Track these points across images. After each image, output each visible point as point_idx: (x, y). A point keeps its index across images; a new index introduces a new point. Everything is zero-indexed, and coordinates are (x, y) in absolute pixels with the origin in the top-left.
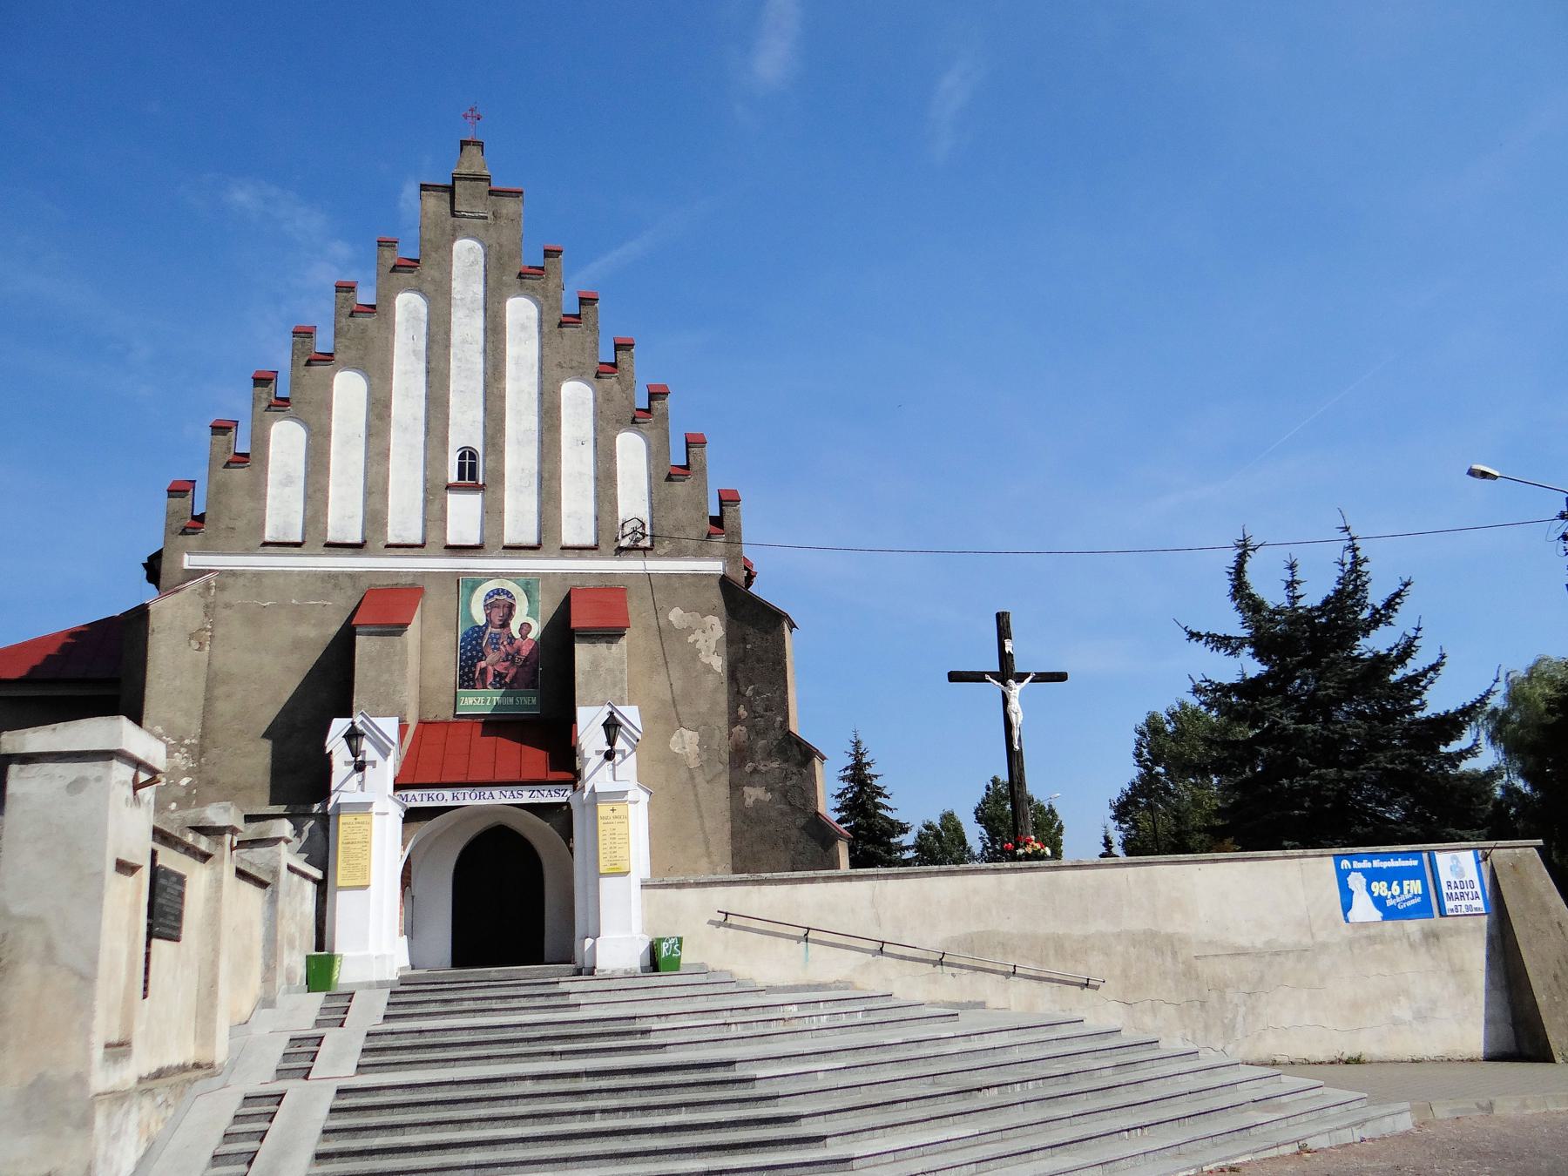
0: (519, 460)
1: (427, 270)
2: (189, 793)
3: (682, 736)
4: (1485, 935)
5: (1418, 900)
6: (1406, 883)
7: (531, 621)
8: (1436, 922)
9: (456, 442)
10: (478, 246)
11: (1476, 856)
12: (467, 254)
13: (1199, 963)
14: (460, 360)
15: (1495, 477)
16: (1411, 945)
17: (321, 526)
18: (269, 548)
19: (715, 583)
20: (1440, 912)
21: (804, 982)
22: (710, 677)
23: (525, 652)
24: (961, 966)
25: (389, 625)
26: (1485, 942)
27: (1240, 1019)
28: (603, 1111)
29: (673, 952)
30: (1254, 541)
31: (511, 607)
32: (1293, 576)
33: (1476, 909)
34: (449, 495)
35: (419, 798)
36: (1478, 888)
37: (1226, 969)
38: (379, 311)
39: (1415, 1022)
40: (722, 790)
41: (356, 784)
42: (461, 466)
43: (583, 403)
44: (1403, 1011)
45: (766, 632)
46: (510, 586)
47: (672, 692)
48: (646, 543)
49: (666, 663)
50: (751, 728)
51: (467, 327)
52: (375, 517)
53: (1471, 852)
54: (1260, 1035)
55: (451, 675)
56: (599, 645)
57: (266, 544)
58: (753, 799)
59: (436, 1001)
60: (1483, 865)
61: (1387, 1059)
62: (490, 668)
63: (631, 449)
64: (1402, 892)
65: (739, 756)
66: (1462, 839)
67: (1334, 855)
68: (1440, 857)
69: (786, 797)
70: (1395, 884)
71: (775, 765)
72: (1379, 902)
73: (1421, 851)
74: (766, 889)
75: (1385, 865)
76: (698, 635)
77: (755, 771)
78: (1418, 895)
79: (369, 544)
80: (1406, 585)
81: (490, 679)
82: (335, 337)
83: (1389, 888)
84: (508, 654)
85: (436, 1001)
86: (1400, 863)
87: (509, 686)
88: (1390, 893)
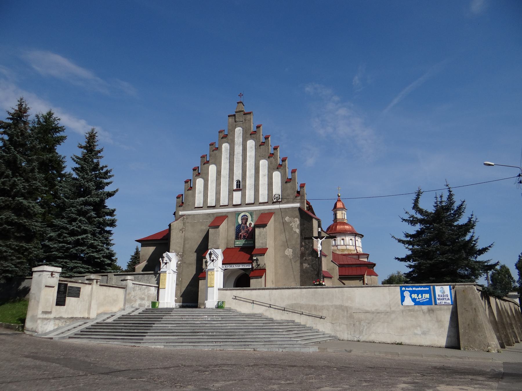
0: (250, 182)
1: (229, 137)
2: (180, 265)
3: (288, 250)
4: (451, 311)
5: (428, 300)
6: (424, 295)
7: (252, 222)
8: (433, 306)
9: (236, 178)
10: (241, 128)
11: (450, 287)
12: (238, 130)
13: (354, 314)
14: (237, 158)
15: (493, 165)
16: (423, 313)
17: (206, 202)
18: (196, 209)
19: (297, 209)
20: (435, 303)
21: (252, 313)
22: (296, 235)
23: (250, 230)
24: (289, 311)
25: (215, 226)
26: (450, 313)
27: (365, 330)
28: (124, 329)
29: (221, 304)
30: (422, 191)
31: (247, 219)
32: (441, 200)
33: (448, 303)
34: (234, 192)
35: (227, 267)
36: (449, 297)
37: (362, 316)
38: (218, 149)
39: (421, 335)
40: (298, 264)
41: (165, 267)
42: (237, 185)
43: (265, 165)
44: (418, 331)
45: (309, 222)
46: (247, 214)
47: (286, 239)
48: (280, 200)
49: (285, 231)
50: (305, 248)
51: (238, 149)
52: (218, 199)
53: (448, 286)
54: (370, 334)
55: (234, 237)
56: (261, 228)
57: (195, 208)
58: (305, 267)
59: (150, 311)
60: (452, 290)
61: (411, 344)
62: (242, 234)
63: (277, 176)
64: (422, 297)
65: (302, 255)
66: (462, 282)
67: (400, 286)
68: (436, 288)
69: (312, 266)
70: (420, 295)
71: (310, 258)
72: (414, 300)
73: (430, 286)
74: (245, 291)
75: (417, 289)
76: (293, 223)
77: (306, 259)
78: (428, 298)
79: (216, 206)
80: (463, 202)
81: (242, 237)
82: (210, 157)
83: (418, 296)
84: (246, 231)
85: (150, 311)
86: (422, 289)
87: (246, 239)
88: (418, 297)
